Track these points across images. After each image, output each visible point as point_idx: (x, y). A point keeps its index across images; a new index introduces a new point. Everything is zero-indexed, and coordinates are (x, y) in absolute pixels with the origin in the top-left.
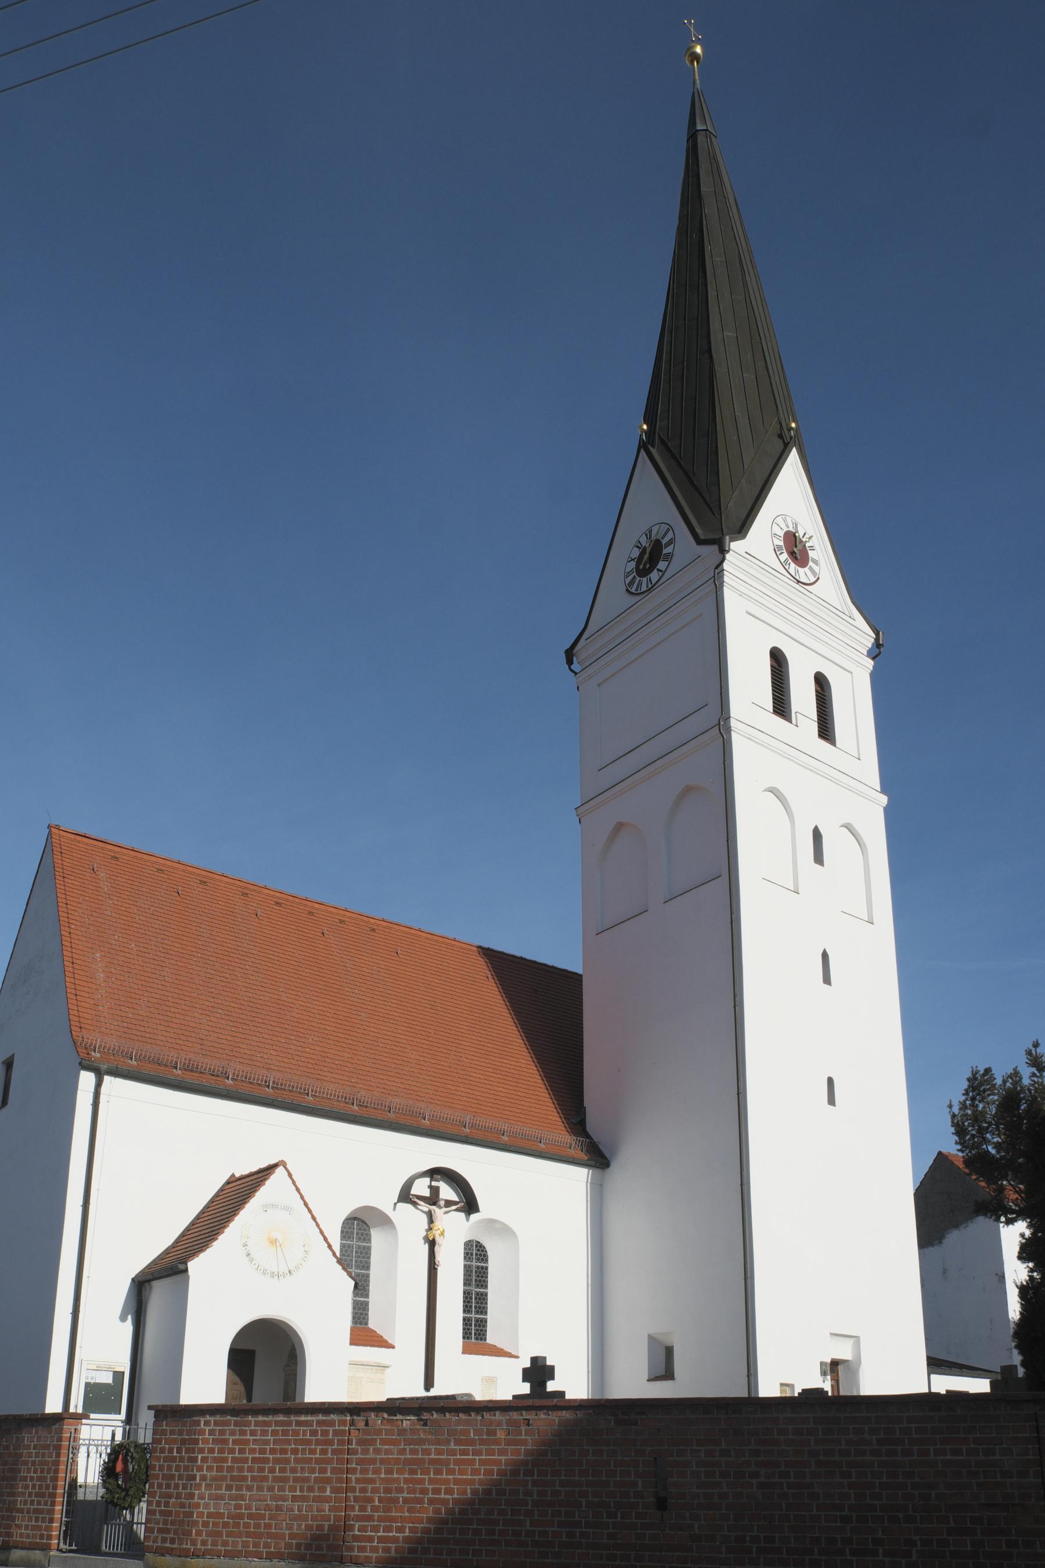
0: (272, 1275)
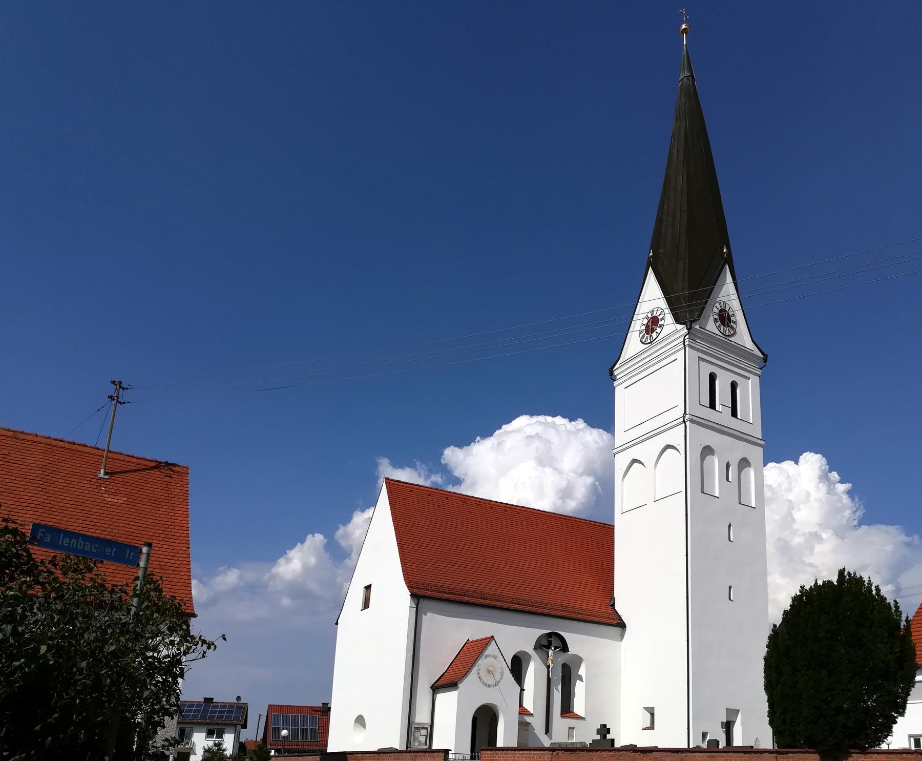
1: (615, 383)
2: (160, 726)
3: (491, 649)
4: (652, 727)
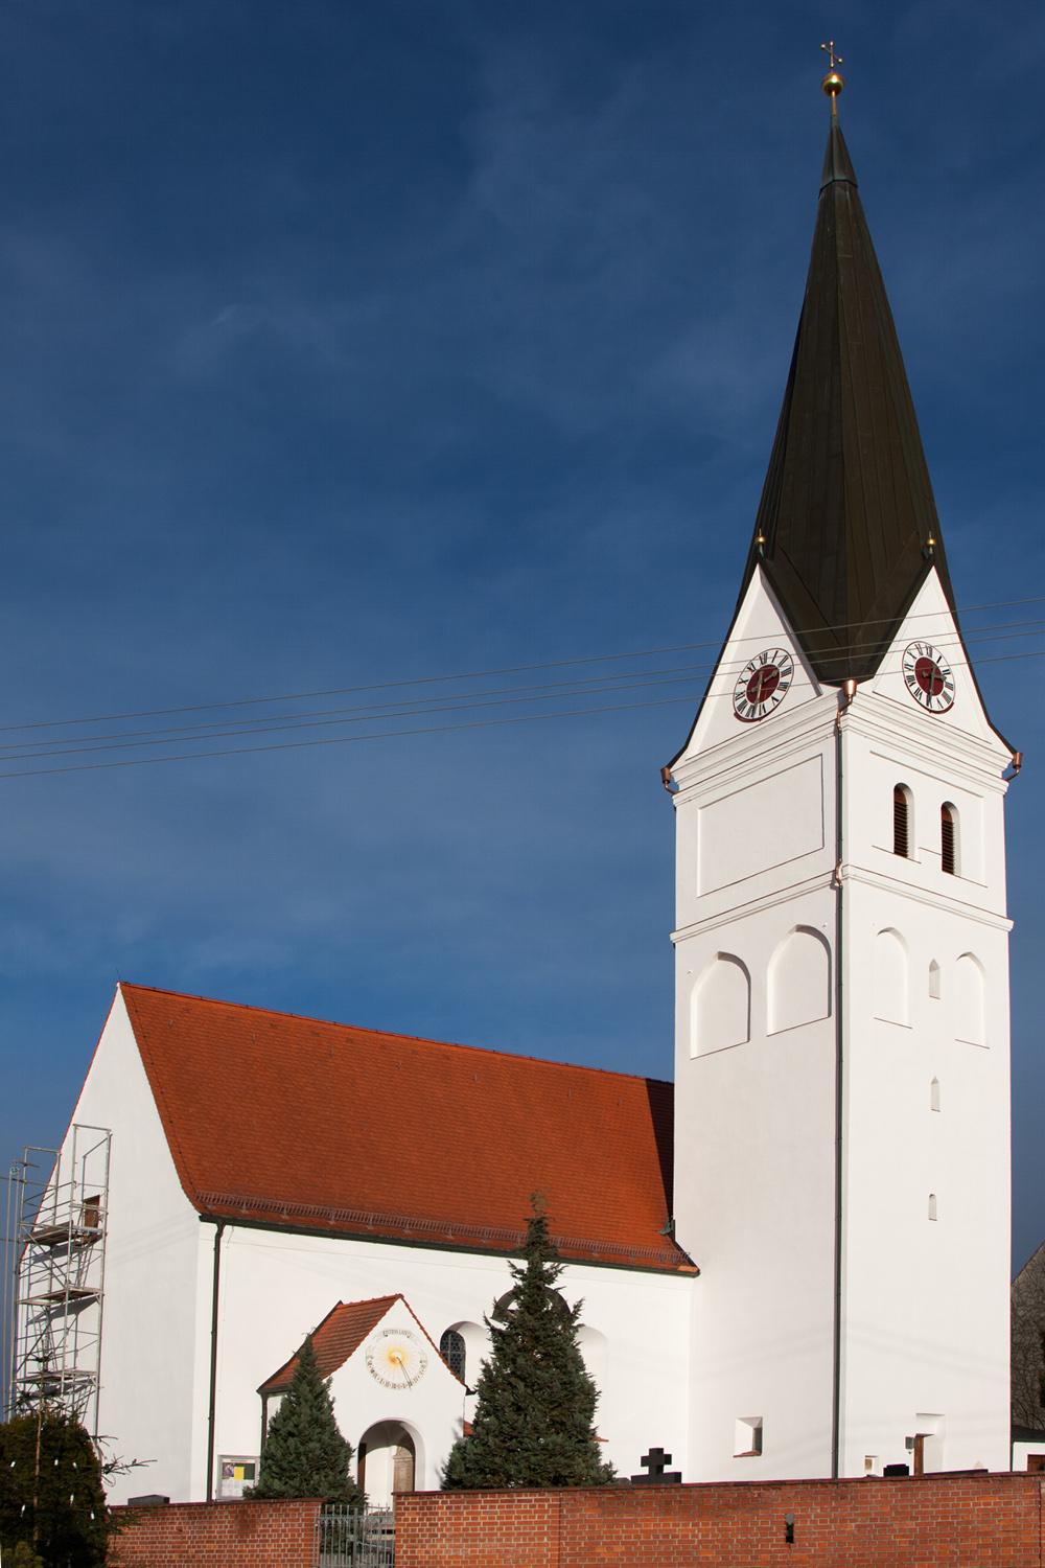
0: (387, 1384)
1: (676, 799)
2: (251, 1494)
3: (395, 1316)
4: (758, 1449)
